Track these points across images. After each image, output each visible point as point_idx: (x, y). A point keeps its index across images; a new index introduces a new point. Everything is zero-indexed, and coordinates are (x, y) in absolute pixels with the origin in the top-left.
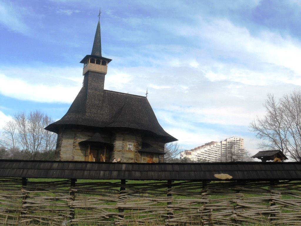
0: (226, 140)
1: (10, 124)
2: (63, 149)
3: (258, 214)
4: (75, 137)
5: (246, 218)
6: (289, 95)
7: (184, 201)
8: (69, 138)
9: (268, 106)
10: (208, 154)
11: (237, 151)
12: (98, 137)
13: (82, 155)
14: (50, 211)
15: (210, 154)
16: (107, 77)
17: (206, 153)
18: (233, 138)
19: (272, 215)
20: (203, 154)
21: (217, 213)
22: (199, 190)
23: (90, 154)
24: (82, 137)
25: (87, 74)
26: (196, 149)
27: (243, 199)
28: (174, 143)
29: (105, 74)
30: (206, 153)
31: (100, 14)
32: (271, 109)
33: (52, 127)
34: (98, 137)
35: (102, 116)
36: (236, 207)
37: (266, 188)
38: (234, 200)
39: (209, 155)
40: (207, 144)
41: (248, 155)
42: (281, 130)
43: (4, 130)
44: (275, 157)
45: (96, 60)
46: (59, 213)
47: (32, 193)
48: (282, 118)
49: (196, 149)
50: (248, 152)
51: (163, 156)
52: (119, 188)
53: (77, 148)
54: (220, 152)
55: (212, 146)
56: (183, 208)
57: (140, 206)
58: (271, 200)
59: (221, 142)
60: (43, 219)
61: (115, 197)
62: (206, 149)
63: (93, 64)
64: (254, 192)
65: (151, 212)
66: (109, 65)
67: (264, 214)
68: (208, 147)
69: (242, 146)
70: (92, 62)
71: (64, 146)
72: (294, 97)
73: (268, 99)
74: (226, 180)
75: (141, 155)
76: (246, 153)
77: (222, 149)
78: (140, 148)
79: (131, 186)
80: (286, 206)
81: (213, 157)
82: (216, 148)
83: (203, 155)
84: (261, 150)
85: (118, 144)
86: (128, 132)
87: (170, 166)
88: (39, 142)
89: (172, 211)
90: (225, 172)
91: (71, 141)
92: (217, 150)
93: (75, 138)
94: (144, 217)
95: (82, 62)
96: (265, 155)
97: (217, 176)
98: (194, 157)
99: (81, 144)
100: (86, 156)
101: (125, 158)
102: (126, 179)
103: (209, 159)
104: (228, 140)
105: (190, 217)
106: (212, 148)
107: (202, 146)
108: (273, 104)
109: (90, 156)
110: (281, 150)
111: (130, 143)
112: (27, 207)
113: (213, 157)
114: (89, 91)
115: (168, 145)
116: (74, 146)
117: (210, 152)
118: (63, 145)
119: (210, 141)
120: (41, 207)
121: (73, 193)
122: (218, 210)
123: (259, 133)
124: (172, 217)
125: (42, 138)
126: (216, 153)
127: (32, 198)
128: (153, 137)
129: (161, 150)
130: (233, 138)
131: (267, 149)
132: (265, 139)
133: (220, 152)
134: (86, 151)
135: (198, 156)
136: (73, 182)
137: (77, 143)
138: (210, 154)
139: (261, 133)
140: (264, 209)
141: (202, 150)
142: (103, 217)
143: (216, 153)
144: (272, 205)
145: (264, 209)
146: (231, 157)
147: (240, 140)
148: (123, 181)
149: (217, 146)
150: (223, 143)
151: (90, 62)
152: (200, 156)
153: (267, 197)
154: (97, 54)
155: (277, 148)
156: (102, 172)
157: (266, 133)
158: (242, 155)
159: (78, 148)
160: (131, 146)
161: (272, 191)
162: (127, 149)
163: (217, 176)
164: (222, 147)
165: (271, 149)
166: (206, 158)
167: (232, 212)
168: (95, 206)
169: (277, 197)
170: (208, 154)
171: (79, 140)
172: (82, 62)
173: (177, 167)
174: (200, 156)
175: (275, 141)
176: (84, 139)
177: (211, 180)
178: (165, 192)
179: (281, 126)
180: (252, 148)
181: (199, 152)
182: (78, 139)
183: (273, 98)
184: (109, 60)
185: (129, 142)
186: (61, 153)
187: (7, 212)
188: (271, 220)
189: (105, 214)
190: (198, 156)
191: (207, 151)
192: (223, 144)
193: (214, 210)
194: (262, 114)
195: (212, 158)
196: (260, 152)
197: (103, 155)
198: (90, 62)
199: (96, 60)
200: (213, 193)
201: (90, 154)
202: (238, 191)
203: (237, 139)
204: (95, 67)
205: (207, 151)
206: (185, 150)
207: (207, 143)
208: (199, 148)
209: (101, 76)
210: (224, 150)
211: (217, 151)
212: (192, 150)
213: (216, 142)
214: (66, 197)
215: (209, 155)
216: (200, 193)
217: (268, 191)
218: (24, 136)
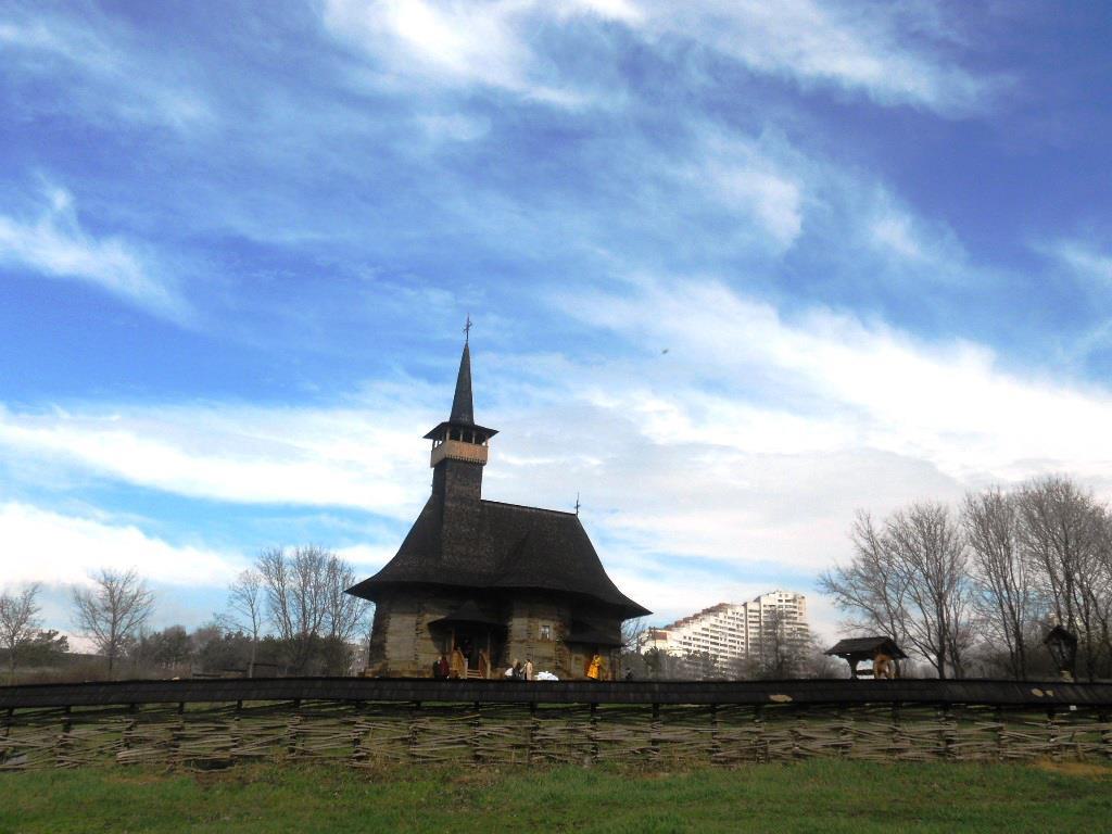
0: (758, 600)
1: (247, 579)
2: (391, 639)
3: (826, 746)
4: (419, 611)
5: (809, 750)
6: (906, 510)
7: (734, 732)
8: (404, 613)
9: (857, 536)
10: (712, 637)
11: (788, 634)
12: (471, 610)
13: (436, 651)
14: (569, 746)
15: (717, 638)
16: (487, 472)
17: (707, 635)
18: (777, 594)
19: (844, 747)
20: (698, 637)
21: (775, 746)
22: (752, 716)
23: (455, 649)
24: (436, 610)
25: (441, 466)
26: (677, 625)
27: (805, 728)
28: (643, 619)
29: (480, 464)
30: (707, 635)
31: (468, 326)
32: (865, 544)
33: (364, 590)
34: (471, 610)
35: (478, 560)
36: (797, 737)
37: (835, 713)
38: (796, 729)
39: (713, 640)
40: (708, 612)
41: (818, 645)
42: (889, 591)
43: (231, 592)
44: (877, 653)
45: (462, 432)
46: (579, 747)
47: (544, 723)
48: (890, 564)
49: (677, 625)
50: (815, 637)
51: (619, 652)
52: (651, 715)
53: (424, 635)
54: (742, 632)
55: (721, 615)
56: (732, 740)
57: (679, 738)
58: (842, 728)
59: (745, 605)
60: (560, 755)
61: (648, 727)
62: (705, 624)
63: (456, 444)
64: (822, 719)
65: (691, 745)
66: (491, 442)
67: (833, 746)
68: (712, 619)
69: (801, 614)
70: (455, 437)
71: (396, 631)
72: (916, 515)
73: (858, 521)
74: (786, 702)
75: (571, 649)
76: (810, 638)
77: (749, 630)
78: (568, 633)
79: (666, 712)
80: (860, 736)
81: (726, 646)
82: (731, 621)
83: (698, 640)
84: (845, 637)
85: (518, 625)
86: (540, 598)
87: (714, 686)
88: (318, 619)
89: (719, 744)
90: (782, 692)
91: (410, 620)
92: (735, 627)
93: (419, 612)
94: (685, 751)
95: (428, 436)
96: (855, 648)
97: (773, 697)
98: (675, 645)
99: (433, 626)
100: (443, 653)
101: (536, 657)
102: (74, 705)
103: (697, 649)
104: (764, 601)
105: (741, 751)
106: (721, 622)
107: (696, 617)
108: (870, 532)
109: (456, 654)
110: (892, 637)
111: (546, 623)
112: (539, 741)
113: (726, 646)
114: (448, 504)
115: (629, 626)
116: (418, 631)
117: (717, 632)
118: (391, 629)
119: (715, 603)
120: (554, 741)
121: (594, 722)
122: (776, 742)
123: (838, 599)
124: (718, 752)
125: (324, 611)
126: (733, 636)
127: (543, 729)
128: (595, 610)
129: (613, 637)
130: (777, 594)
131: (859, 634)
132: (852, 612)
133: (742, 632)
134: (444, 643)
135: (685, 643)
136: (594, 711)
137: (424, 625)
138: (717, 638)
139: (844, 597)
140: (833, 739)
141: (696, 627)
142: (634, 752)
143: (733, 636)
144: (845, 734)
145: (833, 739)
146: (776, 650)
147: (794, 600)
148: (656, 706)
149: (735, 616)
150: (749, 607)
151: (451, 438)
152: (690, 644)
153: (836, 724)
154: (465, 419)
155: (882, 634)
156: (632, 695)
157: (856, 597)
158: (802, 646)
159: (427, 635)
160: (547, 630)
161: (843, 716)
162: (540, 638)
163: (773, 697)
164: (750, 619)
165: (868, 634)
166: (707, 648)
167: (794, 745)
168: (622, 738)
169: (849, 724)
170: (712, 637)
171: (429, 618)
172: (428, 436)
173: (713, 688)
174: (690, 644)
175: (876, 616)
176: (439, 614)
177: (765, 703)
178: (708, 720)
179: (890, 581)
180: (827, 625)
181: (686, 631)
182: (428, 616)
183: (868, 519)
184: (492, 433)
185: (543, 619)
186: (388, 648)
187: (512, 747)
188: (844, 753)
189: (635, 748)
190: (685, 643)
191: (707, 630)
192: (751, 611)
193: (771, 742)
194: (844, 554)
195: (722, 648)
196: (843, 641)
197: (485, 651)
198: (451, 438)
199: (462, 432)
200: (768, 720)
201: (455, 649)
202: (799, 717)
203: (787, 596)
204: (462, 450)
205: (707, 630)
206: (650, 628)
207: (709, 607)
208: (686, 621)
209: (474, 470)
210: (753, 631)
211: (734, 630)
212: (668, 628)
213: (732, 606)
214: (586, 727)
215: (713, 640)
216: (752, 720)
217: (837, 717)
218: (281, 600)
